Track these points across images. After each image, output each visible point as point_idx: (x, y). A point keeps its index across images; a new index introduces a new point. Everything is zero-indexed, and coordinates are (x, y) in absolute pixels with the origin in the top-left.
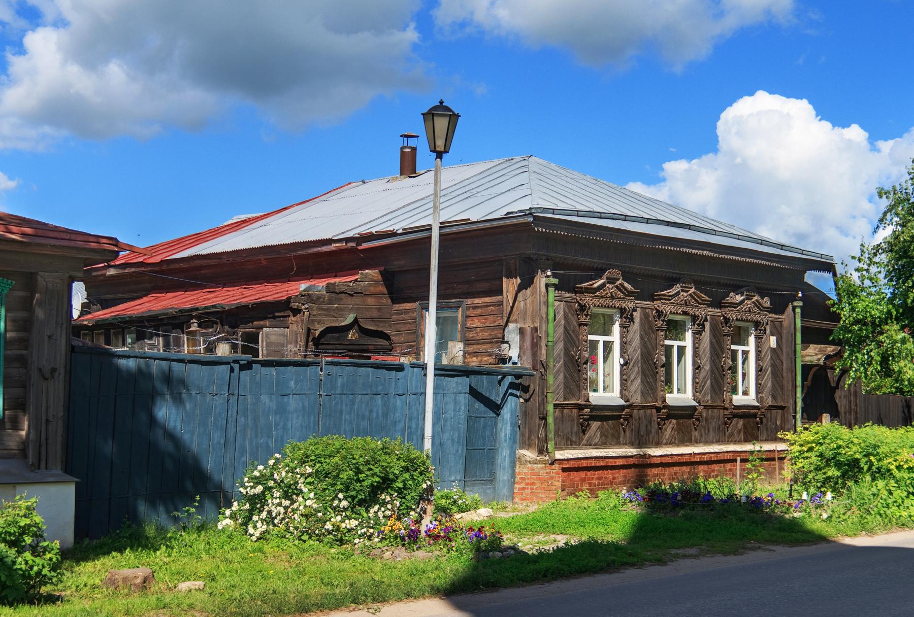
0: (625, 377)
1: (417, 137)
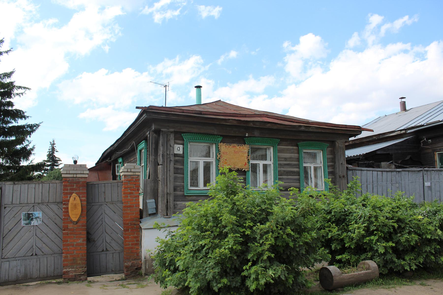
1: (405, 98)
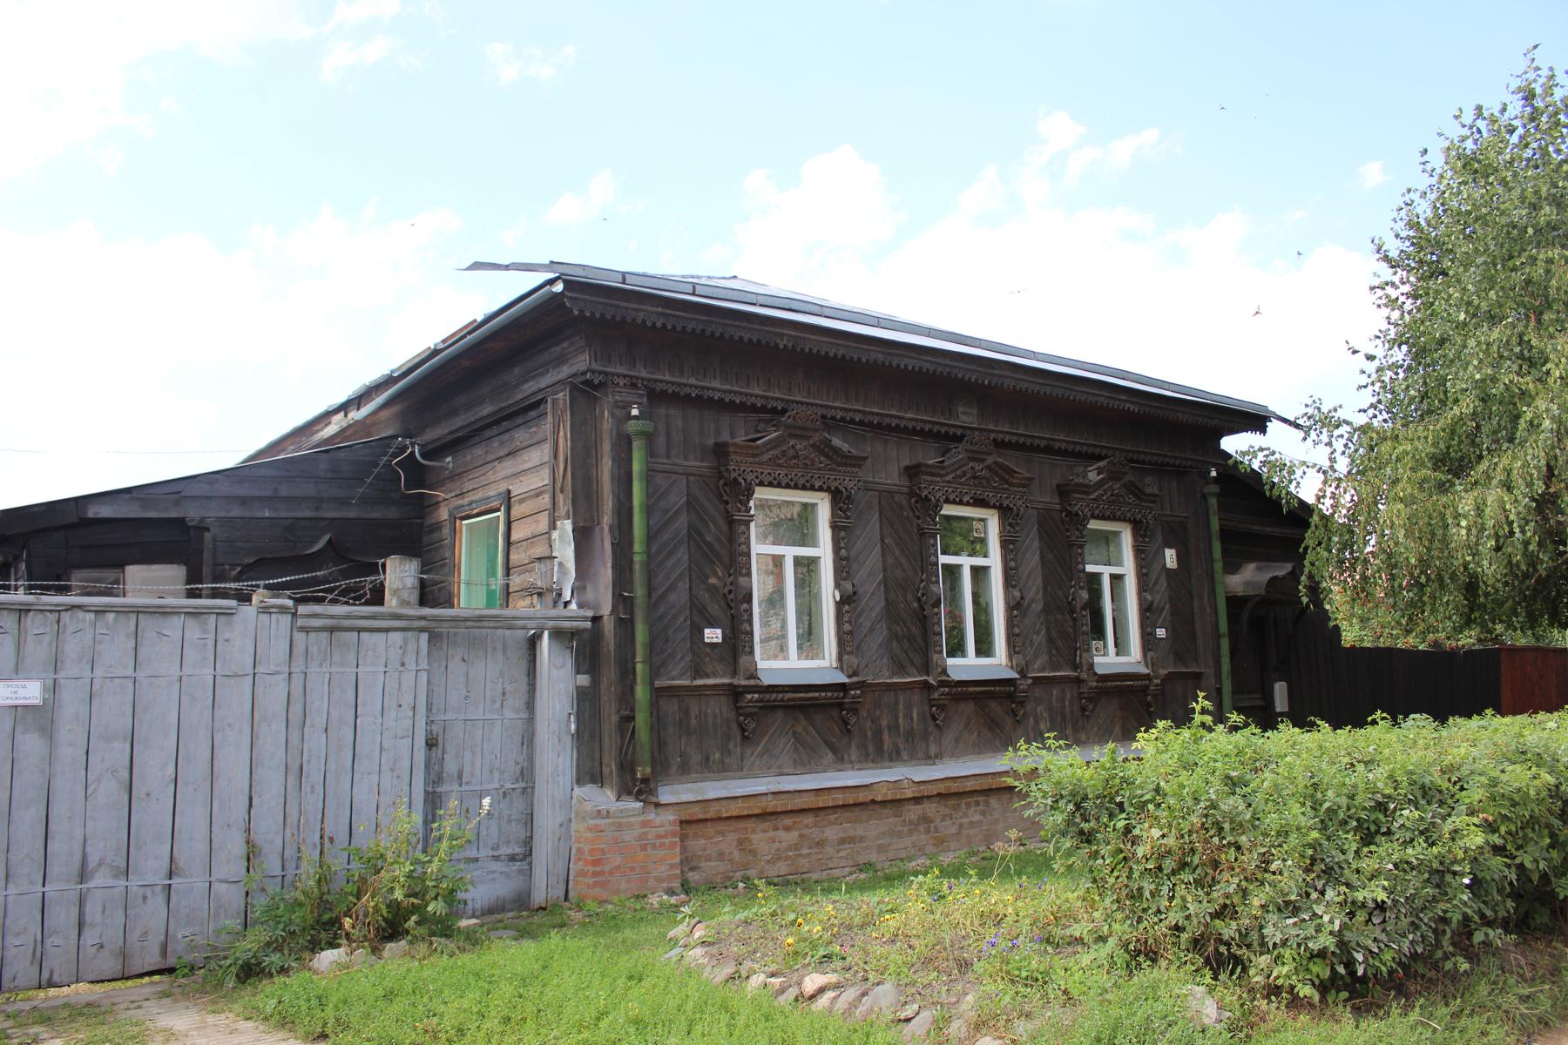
0: (1144, 571)
1: (477, 266)
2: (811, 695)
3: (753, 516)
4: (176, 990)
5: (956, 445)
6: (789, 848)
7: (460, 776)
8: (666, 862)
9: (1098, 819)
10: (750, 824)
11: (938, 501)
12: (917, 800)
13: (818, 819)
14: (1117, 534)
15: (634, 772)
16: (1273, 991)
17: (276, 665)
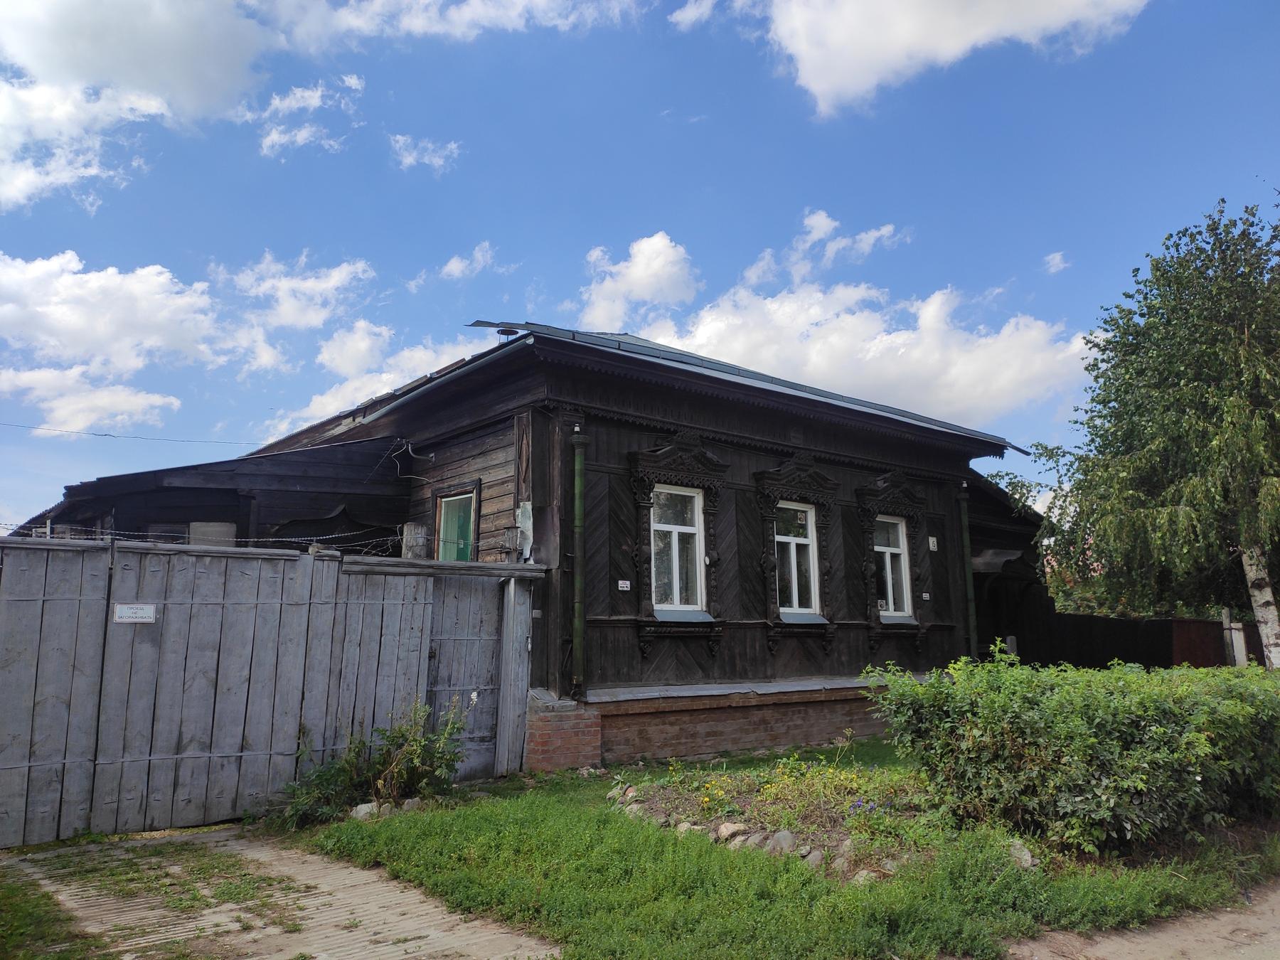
2: (689, 629)
3: (652, 504)
4: (248, 834)
5: (788, 459)
6: (673, 738)
7: (449, 680)
8: (591, 745)
9: (931, 722)
10: (646, 720)
11: (776, 498)
12: (759, 707)
13: (693, 718)
14: (895, 525)
15: (571, 680)
16: (1064, 847)
17: (326, 598)
